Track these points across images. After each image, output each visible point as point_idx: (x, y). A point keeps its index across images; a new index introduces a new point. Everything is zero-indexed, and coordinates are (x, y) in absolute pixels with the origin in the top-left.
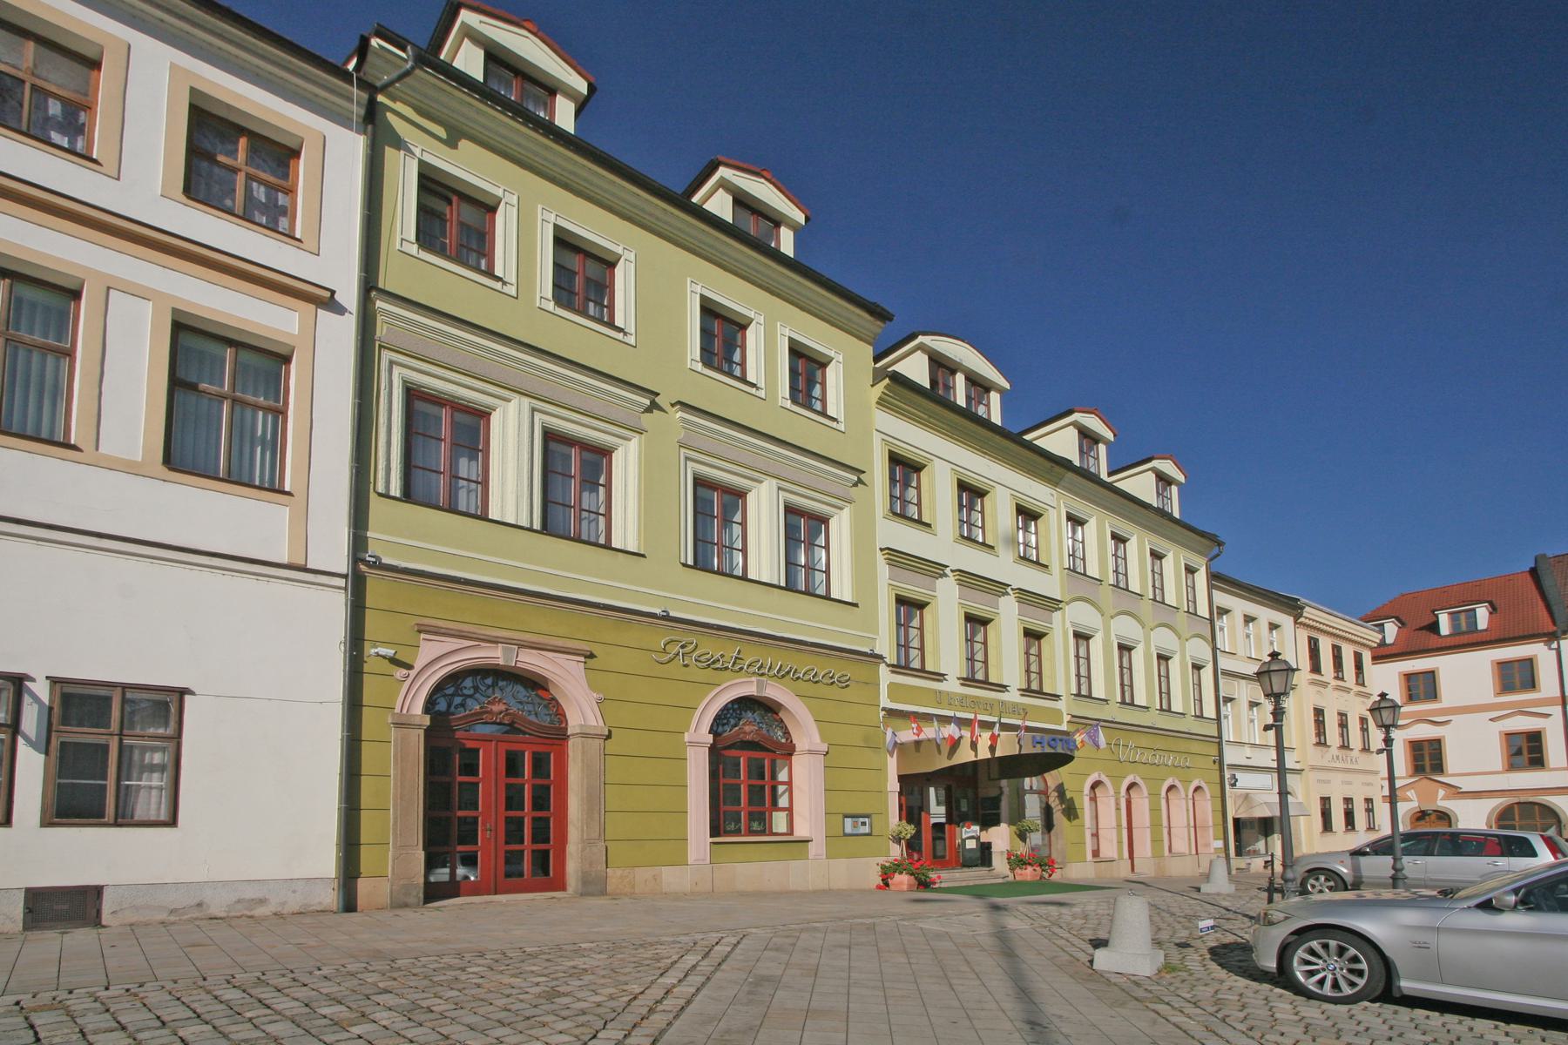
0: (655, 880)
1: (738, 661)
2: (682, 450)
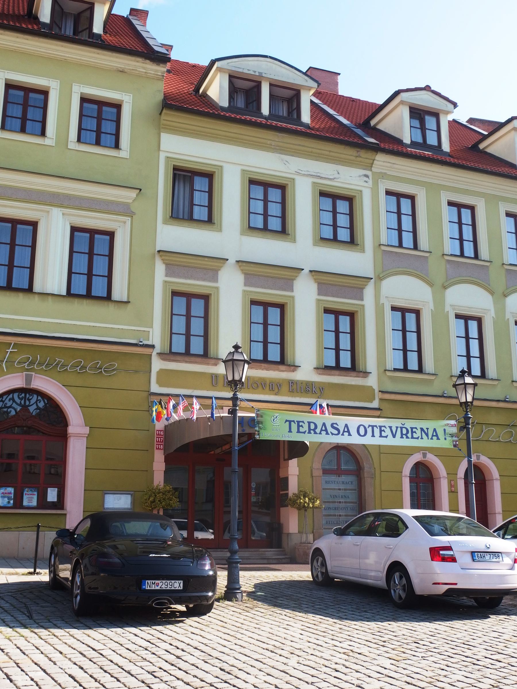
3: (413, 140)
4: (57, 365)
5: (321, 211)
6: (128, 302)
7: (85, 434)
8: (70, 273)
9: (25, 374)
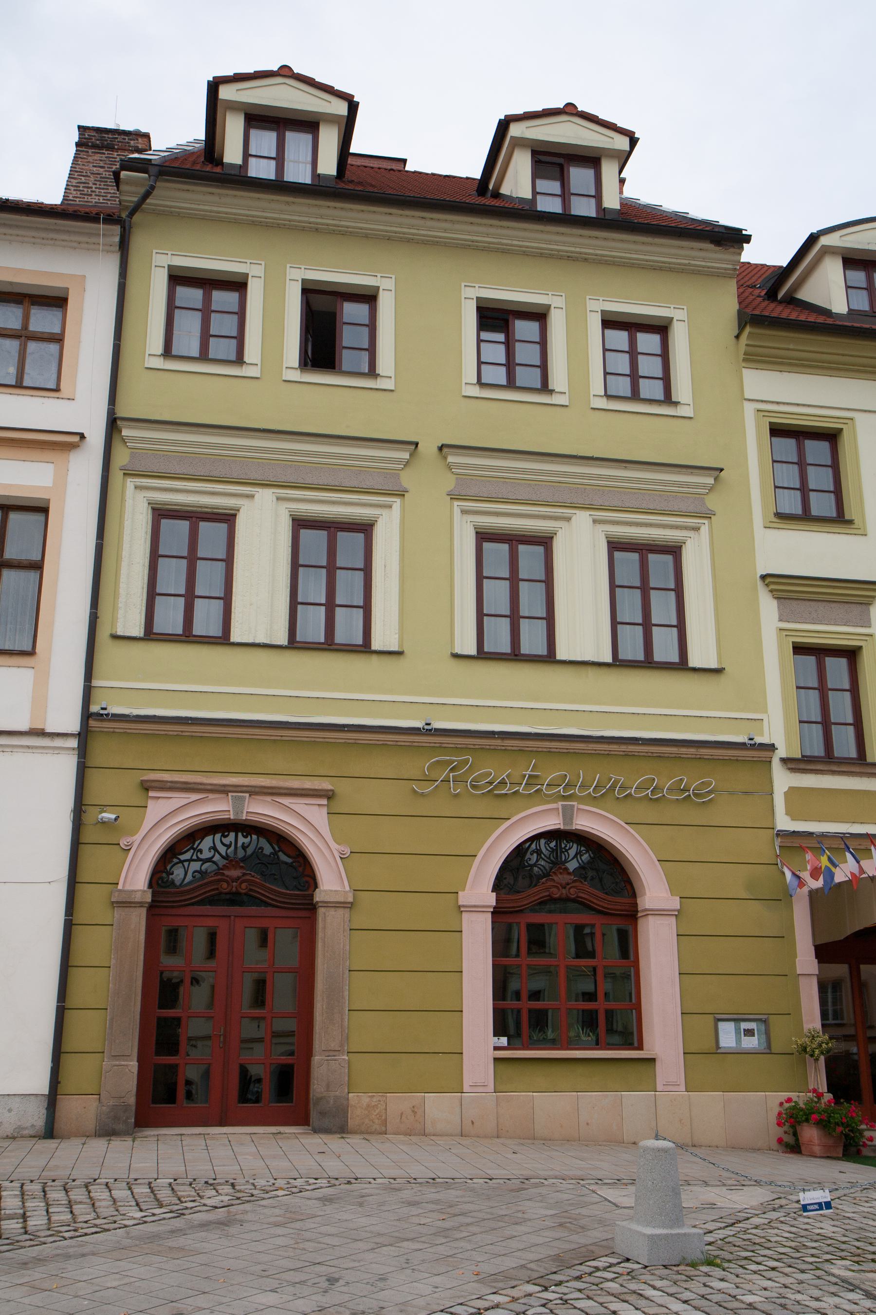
0: (415, 1113)
1: (532, 781)
2: (456, 503)
3: (851, 307)
4: (613, 788)
5: (775, 464)
6: (718, 671)
7: (674, 910)
8: (615, 623)
9: (562, 805)
